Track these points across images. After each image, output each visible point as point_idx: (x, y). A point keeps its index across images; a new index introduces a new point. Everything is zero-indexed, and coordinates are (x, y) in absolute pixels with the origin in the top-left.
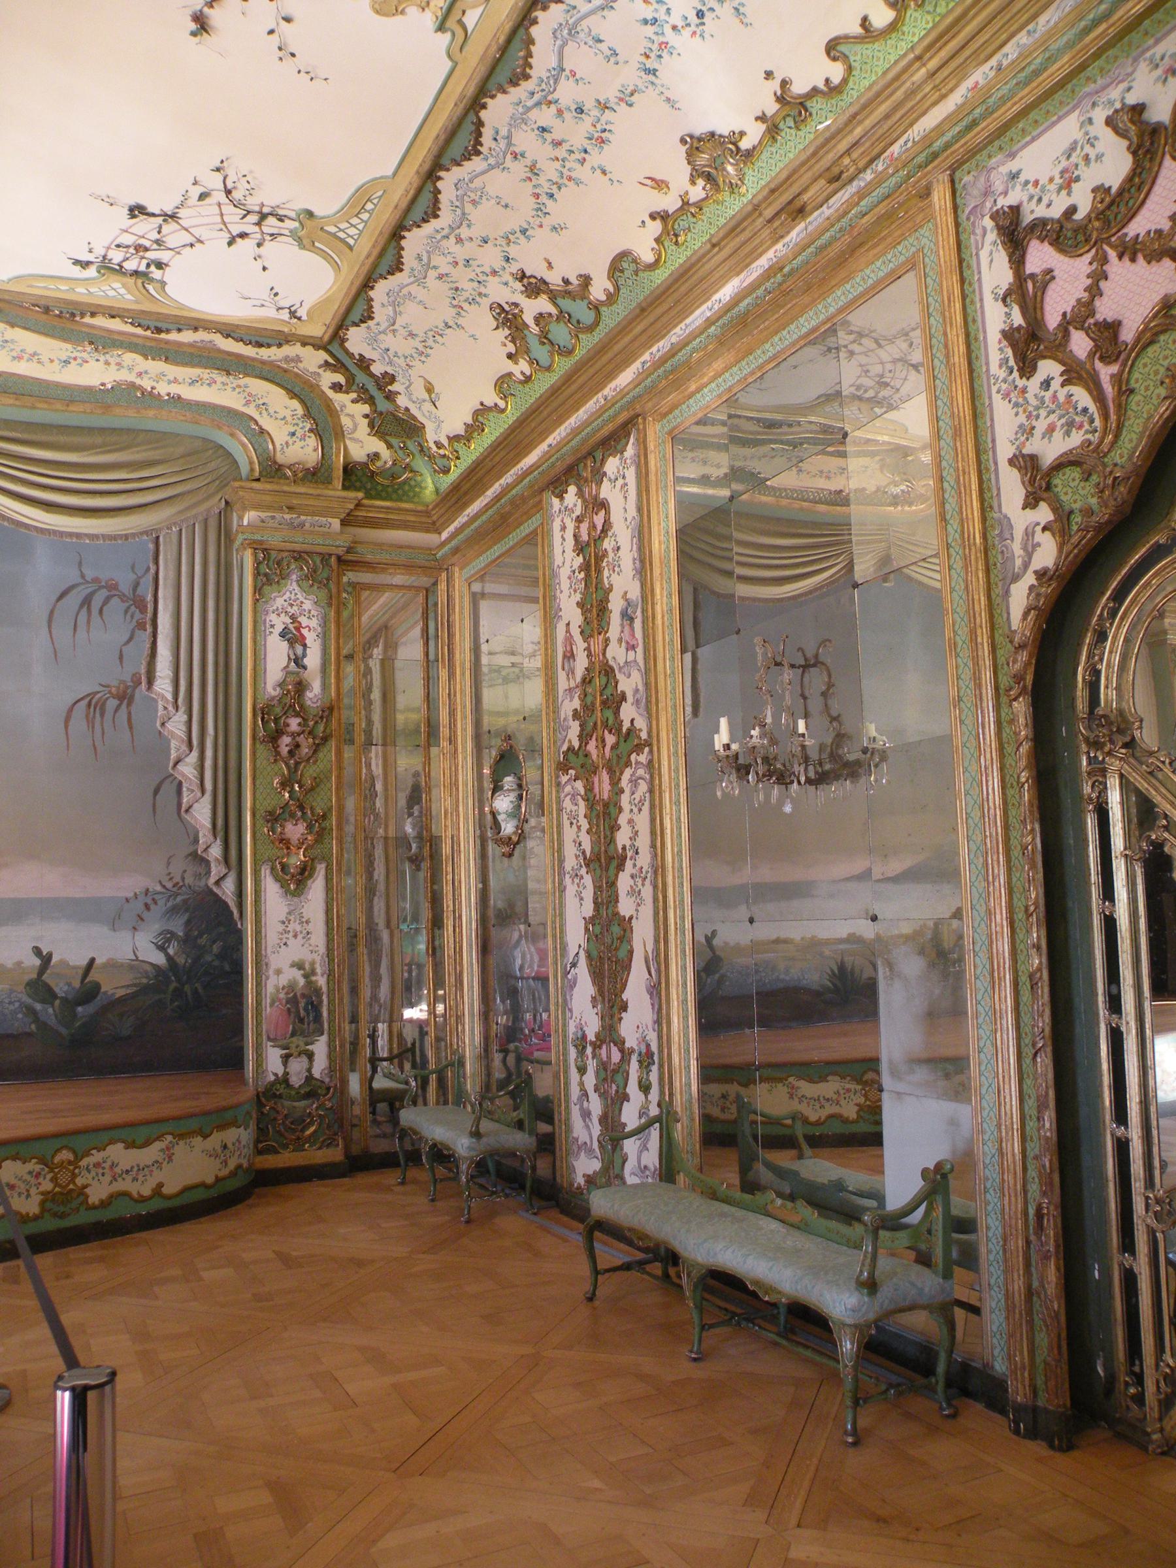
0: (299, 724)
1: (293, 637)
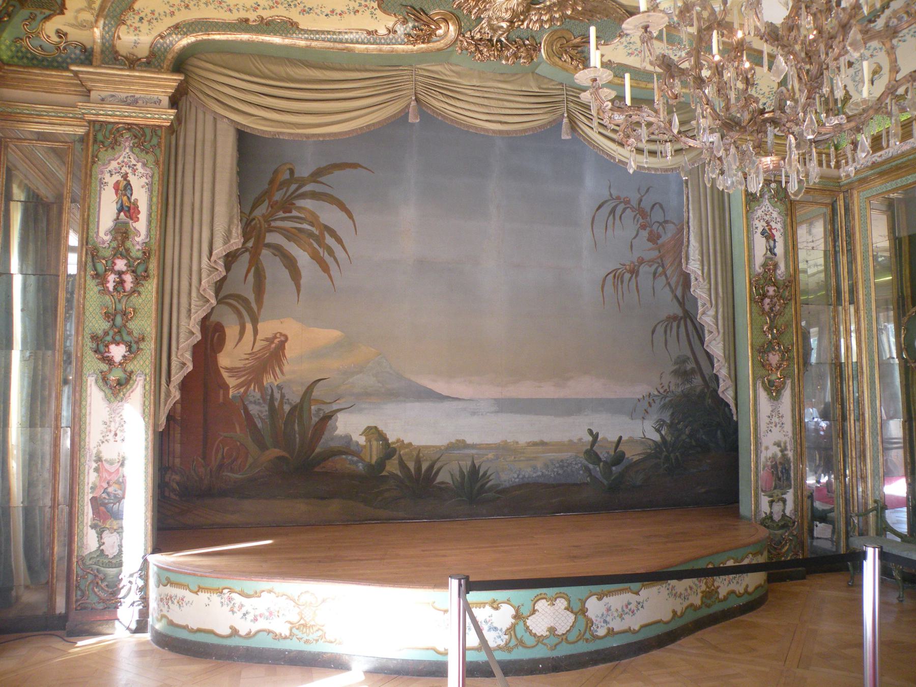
0: (774, 291)
1: (768, 235)
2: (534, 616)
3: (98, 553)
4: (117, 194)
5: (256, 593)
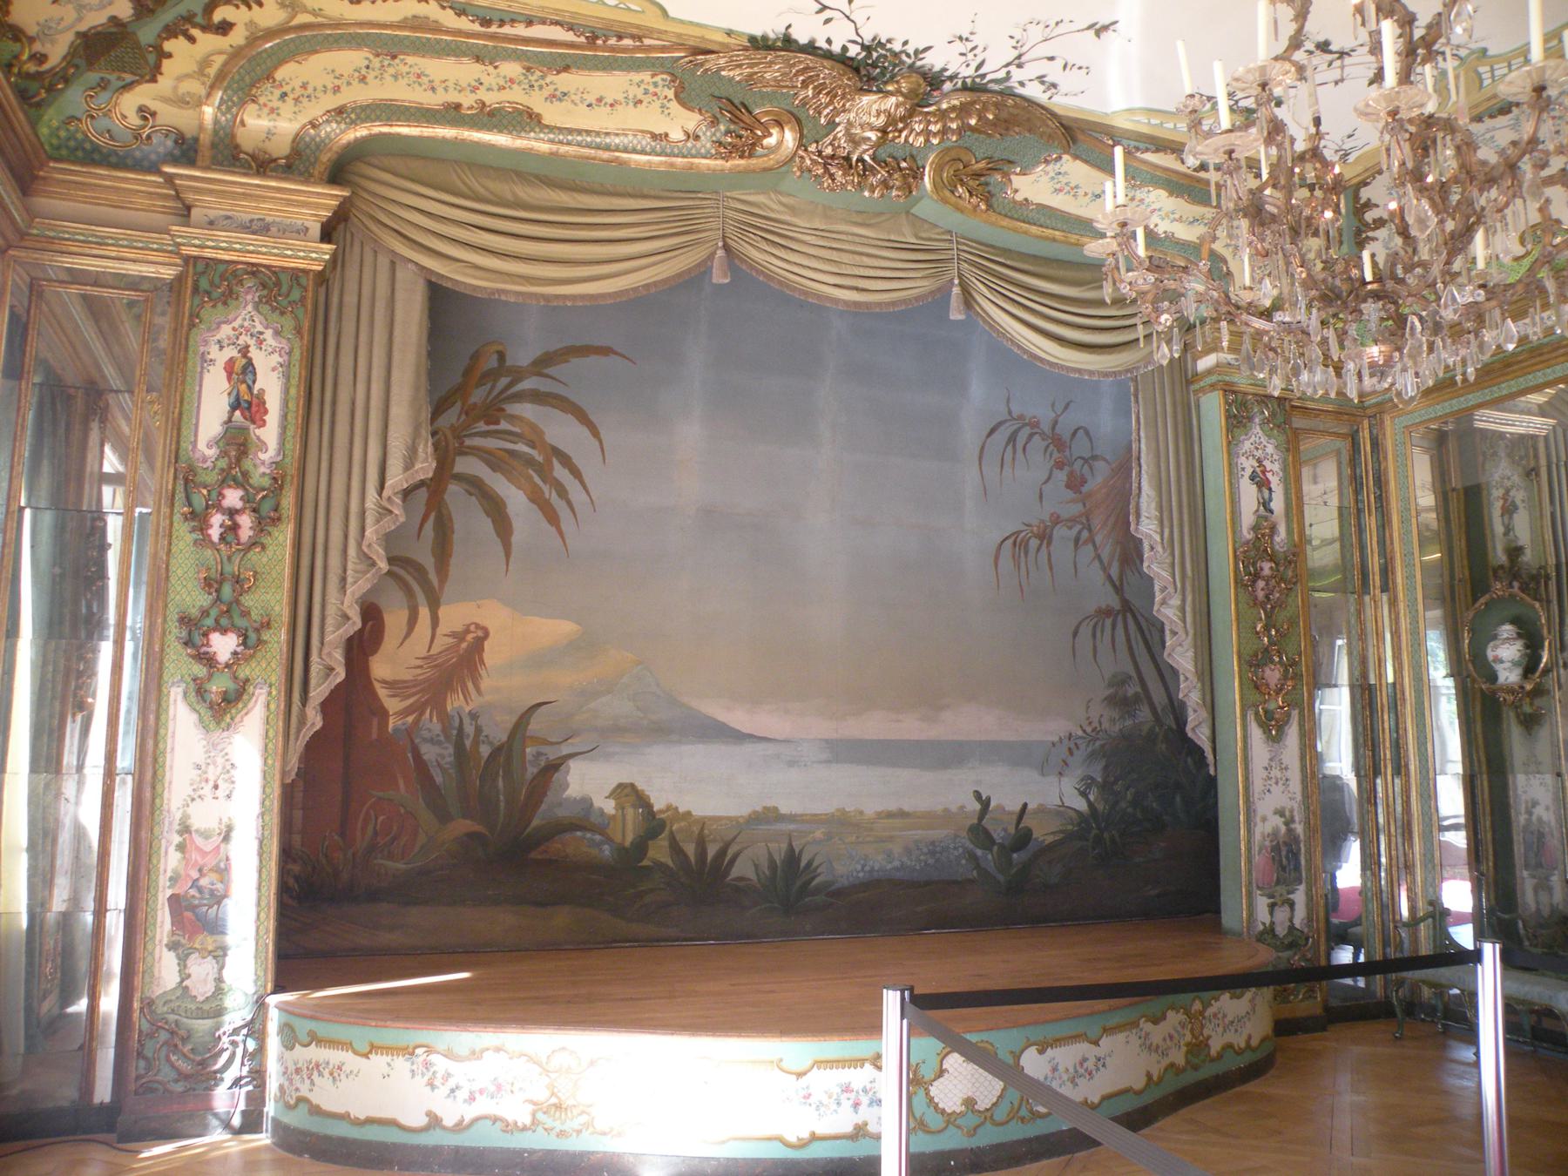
1: (1261, 481)
2: (941, 1080)
3: (179, 993)
4: (229, 378)
5: (473, 1053)
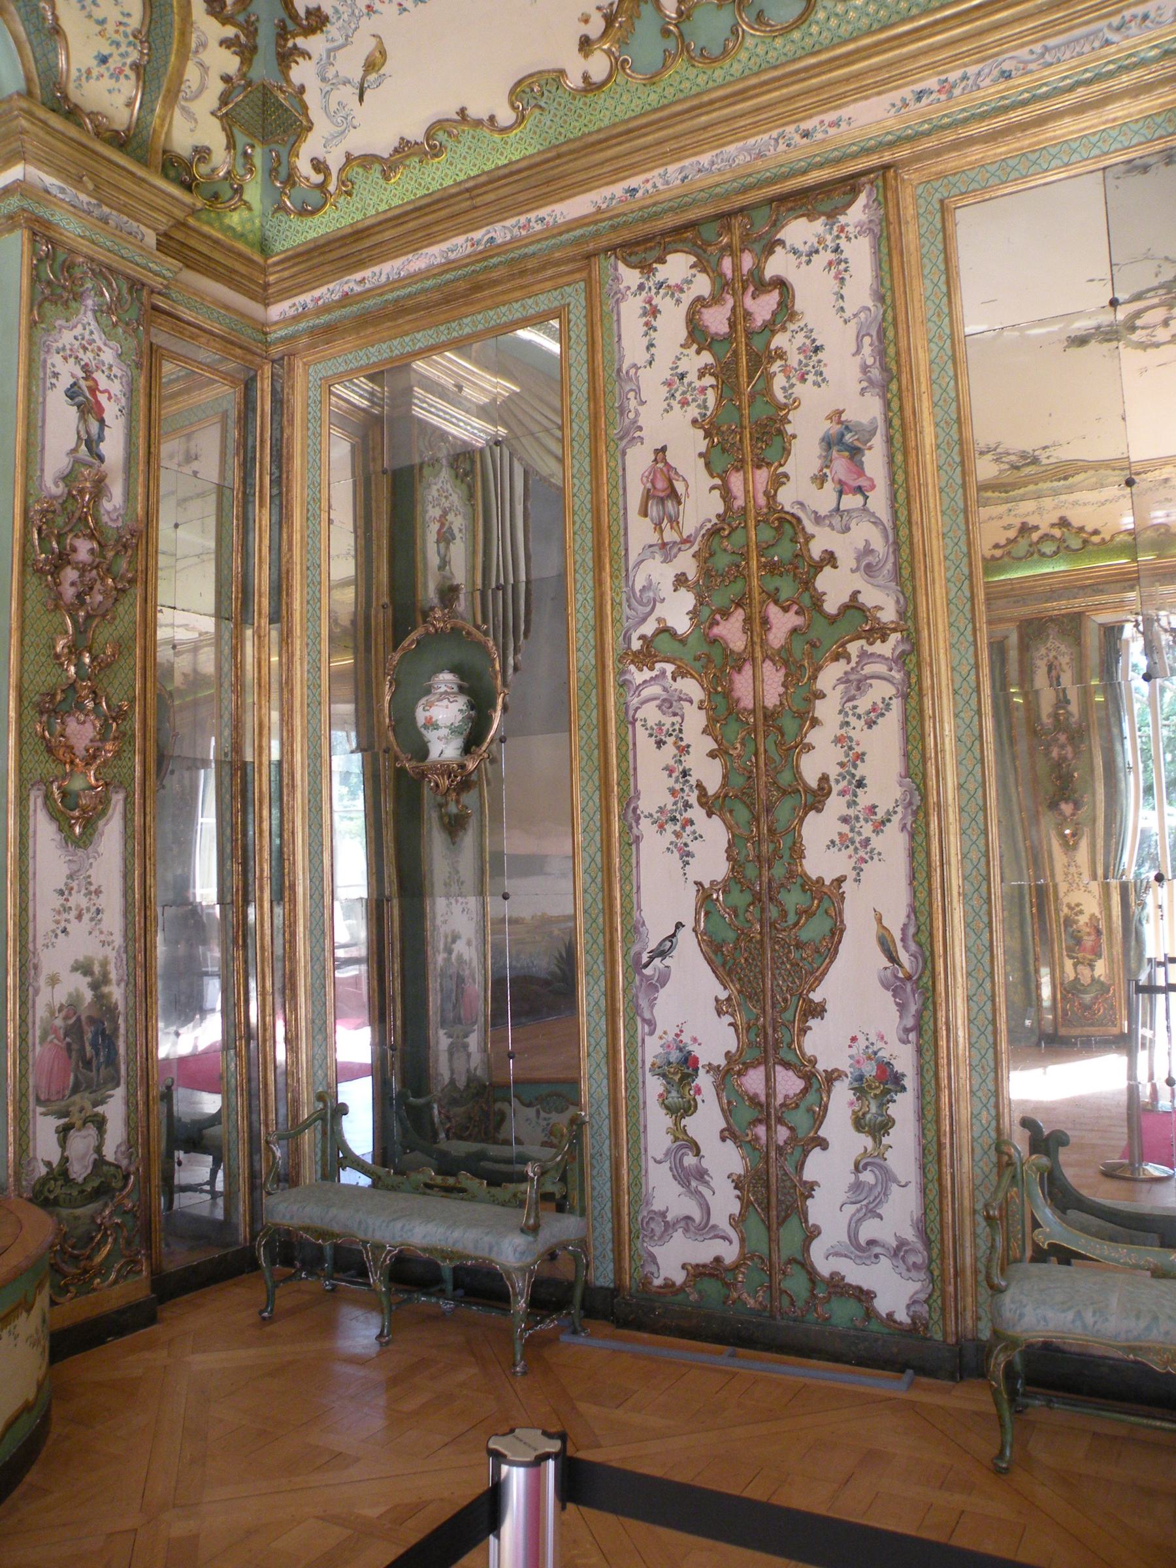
0: (92, 551)
